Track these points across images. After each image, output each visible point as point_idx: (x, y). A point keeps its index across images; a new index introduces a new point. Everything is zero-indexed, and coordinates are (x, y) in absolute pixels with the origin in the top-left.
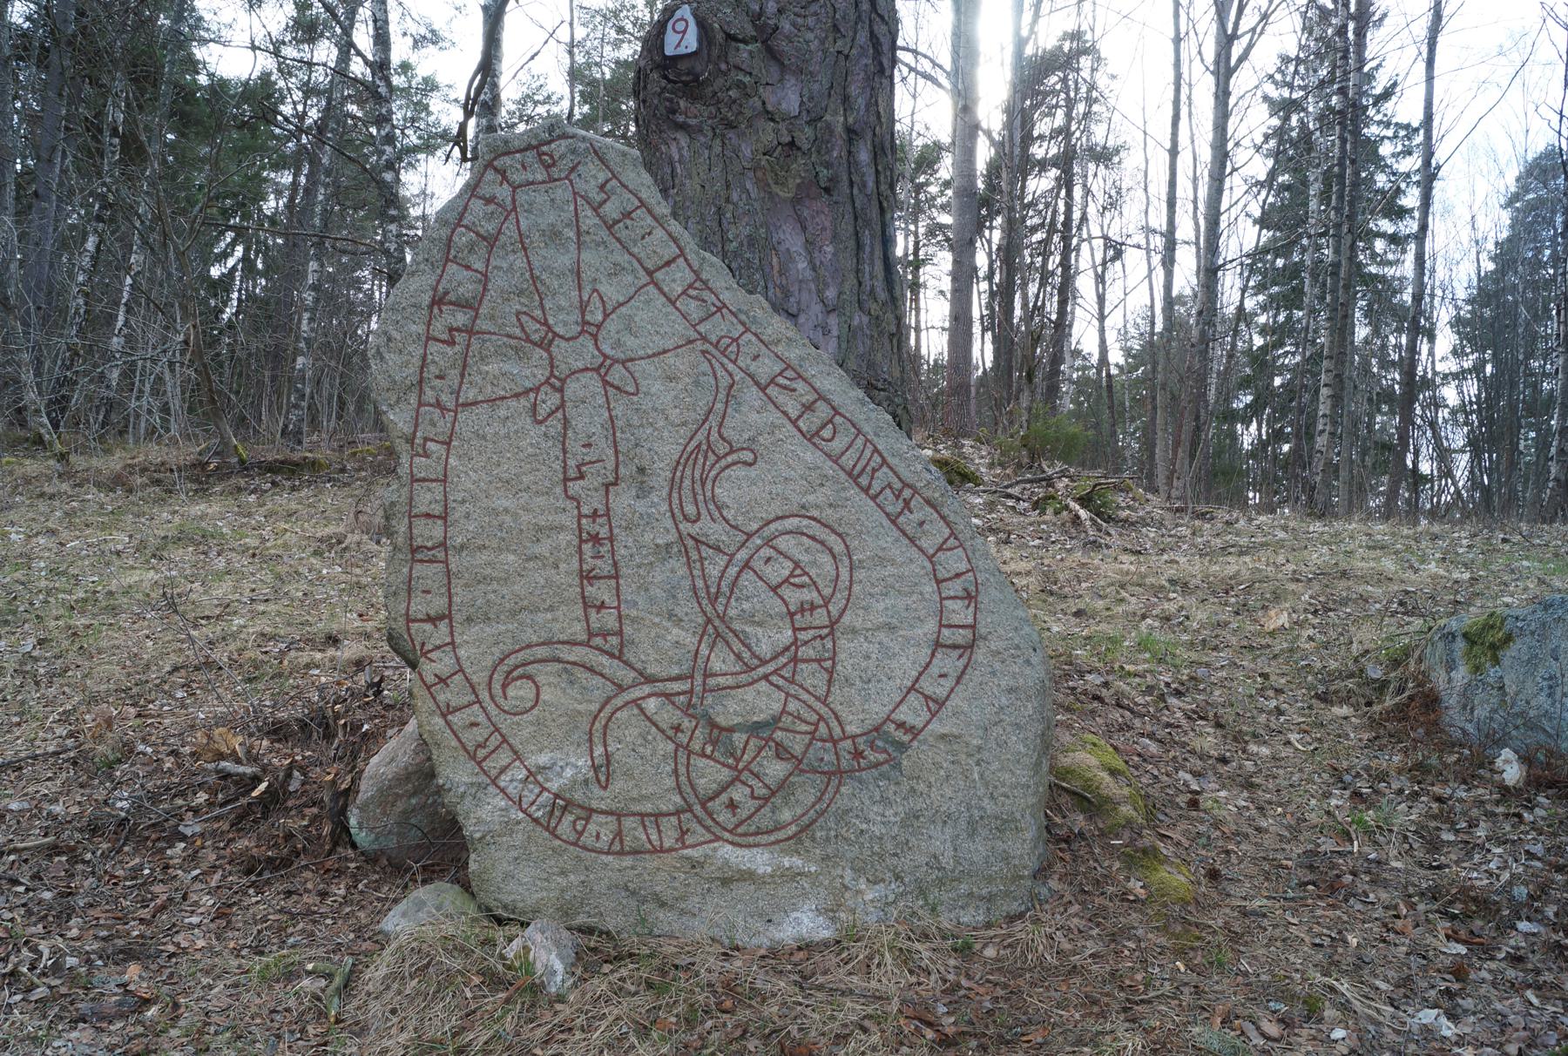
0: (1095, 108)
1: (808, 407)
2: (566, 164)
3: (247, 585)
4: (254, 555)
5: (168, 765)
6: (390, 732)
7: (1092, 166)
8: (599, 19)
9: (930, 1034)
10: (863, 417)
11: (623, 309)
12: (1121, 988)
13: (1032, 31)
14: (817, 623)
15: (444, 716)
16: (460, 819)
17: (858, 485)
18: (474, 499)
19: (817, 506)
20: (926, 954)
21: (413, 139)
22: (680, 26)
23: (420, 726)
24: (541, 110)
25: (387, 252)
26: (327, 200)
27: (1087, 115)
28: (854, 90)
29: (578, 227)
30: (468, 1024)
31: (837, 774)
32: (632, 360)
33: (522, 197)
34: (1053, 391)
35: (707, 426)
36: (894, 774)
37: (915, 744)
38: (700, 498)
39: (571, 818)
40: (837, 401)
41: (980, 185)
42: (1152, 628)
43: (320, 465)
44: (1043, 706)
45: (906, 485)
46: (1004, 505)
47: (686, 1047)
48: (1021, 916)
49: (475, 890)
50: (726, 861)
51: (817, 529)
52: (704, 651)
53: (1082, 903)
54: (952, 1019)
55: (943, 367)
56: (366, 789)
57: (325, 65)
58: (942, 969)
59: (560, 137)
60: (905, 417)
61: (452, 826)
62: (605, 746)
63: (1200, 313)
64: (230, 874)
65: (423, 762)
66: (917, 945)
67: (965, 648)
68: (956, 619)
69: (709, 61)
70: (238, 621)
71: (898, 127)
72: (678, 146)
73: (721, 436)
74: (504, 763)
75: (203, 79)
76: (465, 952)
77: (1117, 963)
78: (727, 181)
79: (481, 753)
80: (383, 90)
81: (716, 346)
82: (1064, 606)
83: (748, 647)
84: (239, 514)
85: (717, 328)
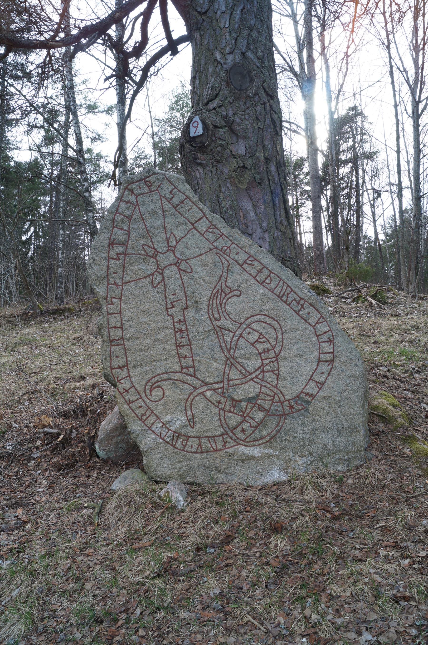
0: (365, 137)
1: (260, 271)
2: (156, 185)
3: (48, 359)
4: (49, 347)
5: (25, 431)
6: (108, 412)
7: (365, 161)
8: (163, 123)
9: (329, 515)
11: (183, 240)
12: (404, 492)
13: (336, 109)
14: (271, 356)
15: (128, 404)
16: (138, 444)
17: (282, 300)
20: (324, 484)
21: (95, 178)
22: (195, 125)
23: (120, 409)
24: (143, 161)
25: (89, 224)
26: (64, 206)
27: (361, 140)
28: (266, 142)
29: (163, 209)
30: (148, 523)
32: (189, 259)
33: (140, 199)
34: (357, 253)
35: (220, 282)
37: (314, 401)
38: (220, 311)
39: (181, 440)
40: (271, 268)
41: (320, 173)
42: (405, 346)
43: (71, 309)
44: (363, 382)
45: (301, 299)
46: (341, 301)
48: (361, 466)
49: (146, 471)
50: (243, 453)
51: (267, 319)
52: (227, 371)
53: (386, 459)
54: (337, 509)
56: (101, 435)
57: (58, 154)
58: (331, 489)
59: (152, 174)
60: (298, 270)
61: (135, 447)
62: (192, 411)
63: (415, 216)
64: (52, 471)
66: (321, 481)
69: (208, 137)
70: (46, 373)
71: (285, 153)
72: (199, 172)
74: (153, 421)
75: (12, 164)
76: (145, 496)
77: (402, 482)
79: (144, 418)
80: (81, 161)
82: (369, 340)
83: (244, 368)
84: (42, 331)
85: (221, 243)
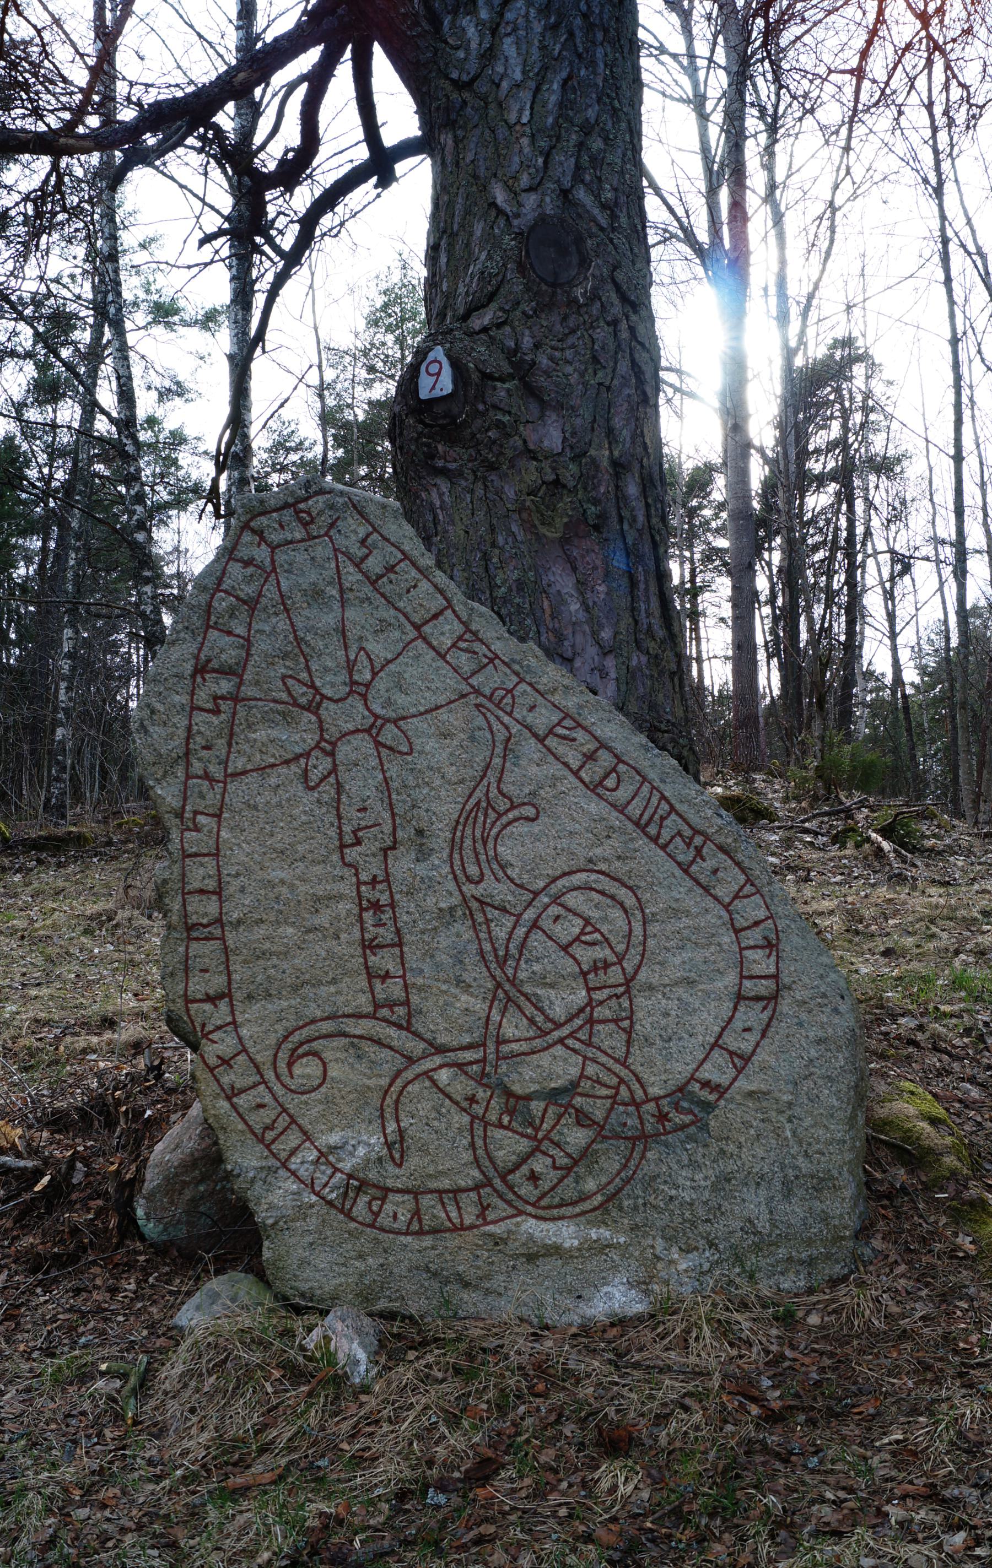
0: (872, 417)
1: (590, 757)
2: (324, 520)
3: (17, 970)
4: (23, 937)
6: (173, 1117)
7: (872, 478)
8: (348, 359)
9: (755, 1410)
10: (647, 763)
11: (392, 667)
12: (956, 1352)
14: (612, 981)
15: (229, 1098)
16: (251, 1205)
17: (646, 834)
18: (249, 871)
19: (605, 860)
20: (746, 1325)
21: (163, 495)
22: (434, 368)
24: (294, 457)
25: (143, 615)
28: (617, 422)
29: (340, 584)
30: (270, 1421)
31: (643, 1138)
32: (404, 718)
33: (281, 557)
34: (846, 716)
35: (485, 782)
36: (703, 1136)
37: (722, 1103)
39: (366, 1198)
40: (619, 747)
41: (756, 505)
42: (966, 964)
43: (86, 839)
45: (697, 832)
47: (499, 1434)
48: (845, 1279)
50: (531, 1237)
52: (496, 1017)
54: (777, 1393)
55: (728, 697)
56: (152, 1178)
58: (764, 1340)
62: (398, 1121)
64: (16, 1273)
65: (209, 1147)
66: (737, 1316)
67: (769, 999)
68: (758, 970)
71: (666, 450)
73: (500, 792)
76: (266, 1346)
78: (491, 525)
79: (270, 1135)
80: (130, 449)
81: (490, 699)
85: (489, 680)
